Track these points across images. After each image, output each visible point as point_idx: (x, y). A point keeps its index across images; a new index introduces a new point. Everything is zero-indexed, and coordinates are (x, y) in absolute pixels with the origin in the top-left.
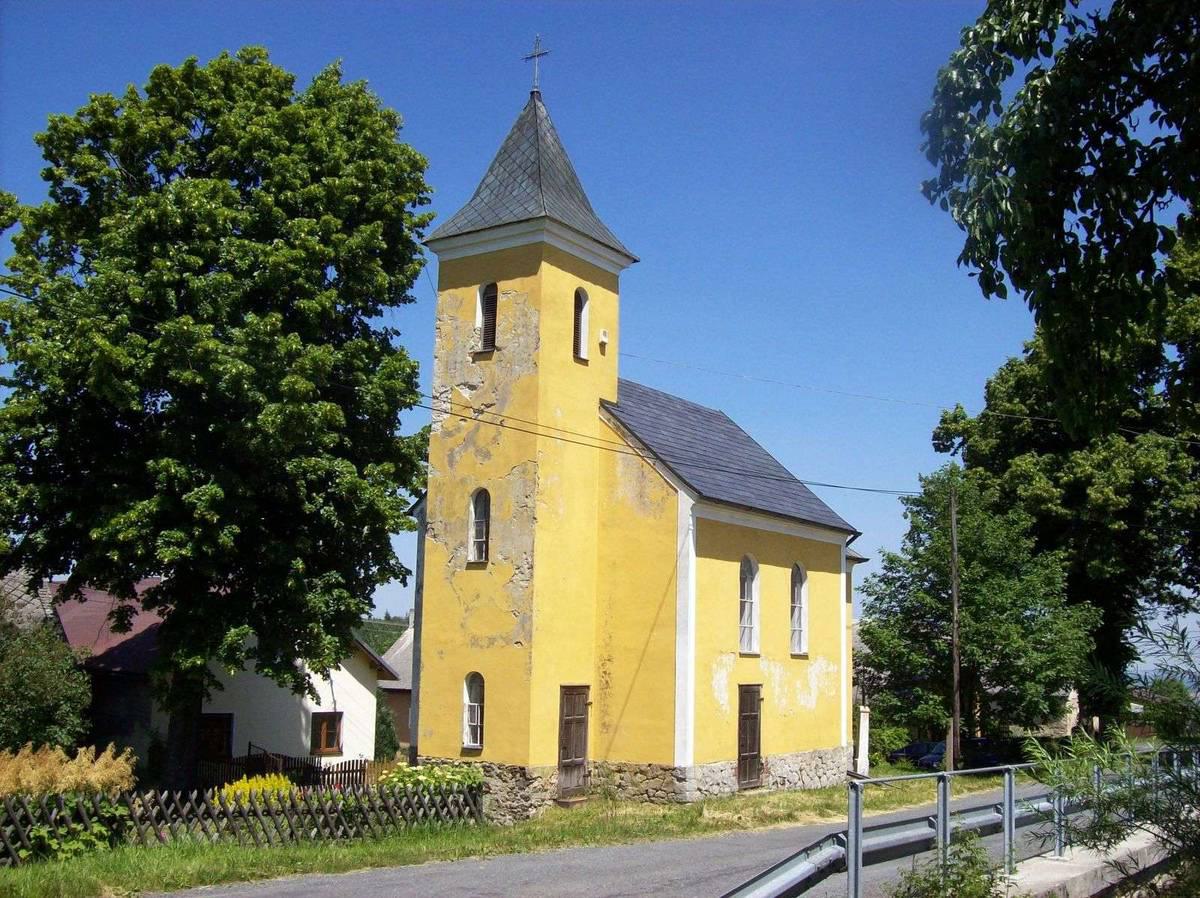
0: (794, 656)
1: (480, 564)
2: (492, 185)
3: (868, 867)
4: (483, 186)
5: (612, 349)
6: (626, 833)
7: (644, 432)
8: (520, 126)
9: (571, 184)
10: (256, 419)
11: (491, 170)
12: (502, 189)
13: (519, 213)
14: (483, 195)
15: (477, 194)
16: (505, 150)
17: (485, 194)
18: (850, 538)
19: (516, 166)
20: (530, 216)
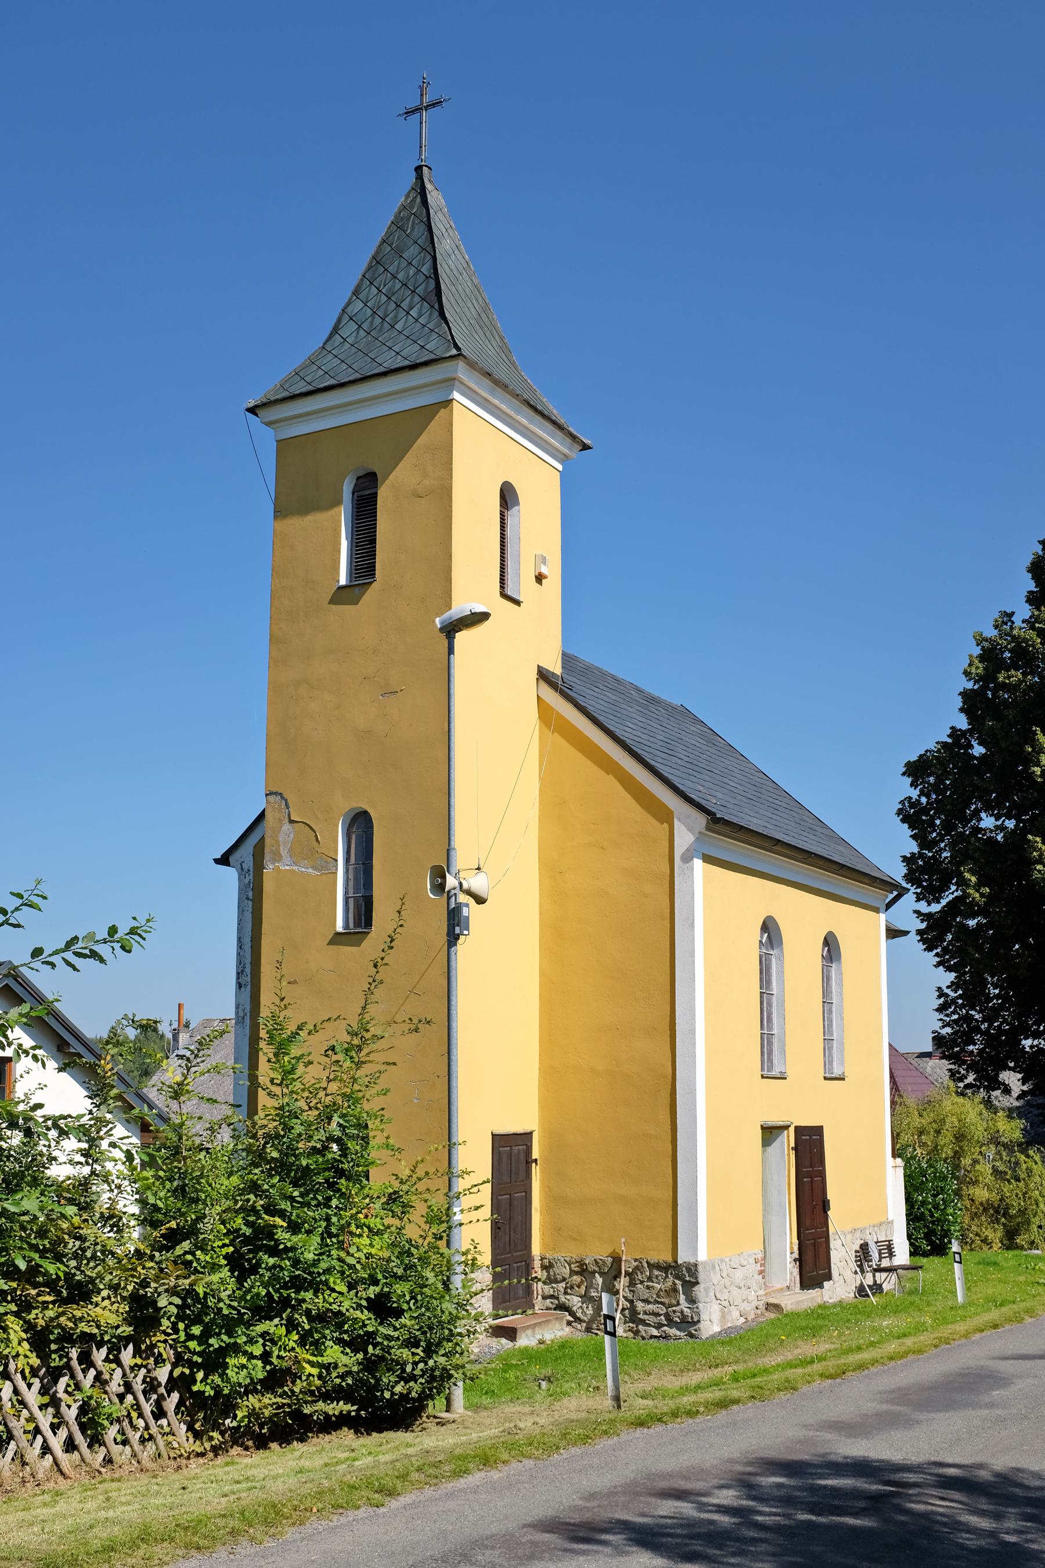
0: (825, 1078)
1: (763, 1077)
2: (359, 316)
3: (519, 1129)
4: (346, 318)
5: (553, 571)
6: (691, 1414)
7: (597, 706)
8: (398, 224)
9: (484, 316)
10: (1010, 835)
11: (356, 293)
12: (378, 321)
13: (412, 353)
14: (345, 332)
15: (335, 330)
16: (377, 260)
17: (348, 329)
18: (891, 896)
19: (398, 285)
20: (433, 356)
